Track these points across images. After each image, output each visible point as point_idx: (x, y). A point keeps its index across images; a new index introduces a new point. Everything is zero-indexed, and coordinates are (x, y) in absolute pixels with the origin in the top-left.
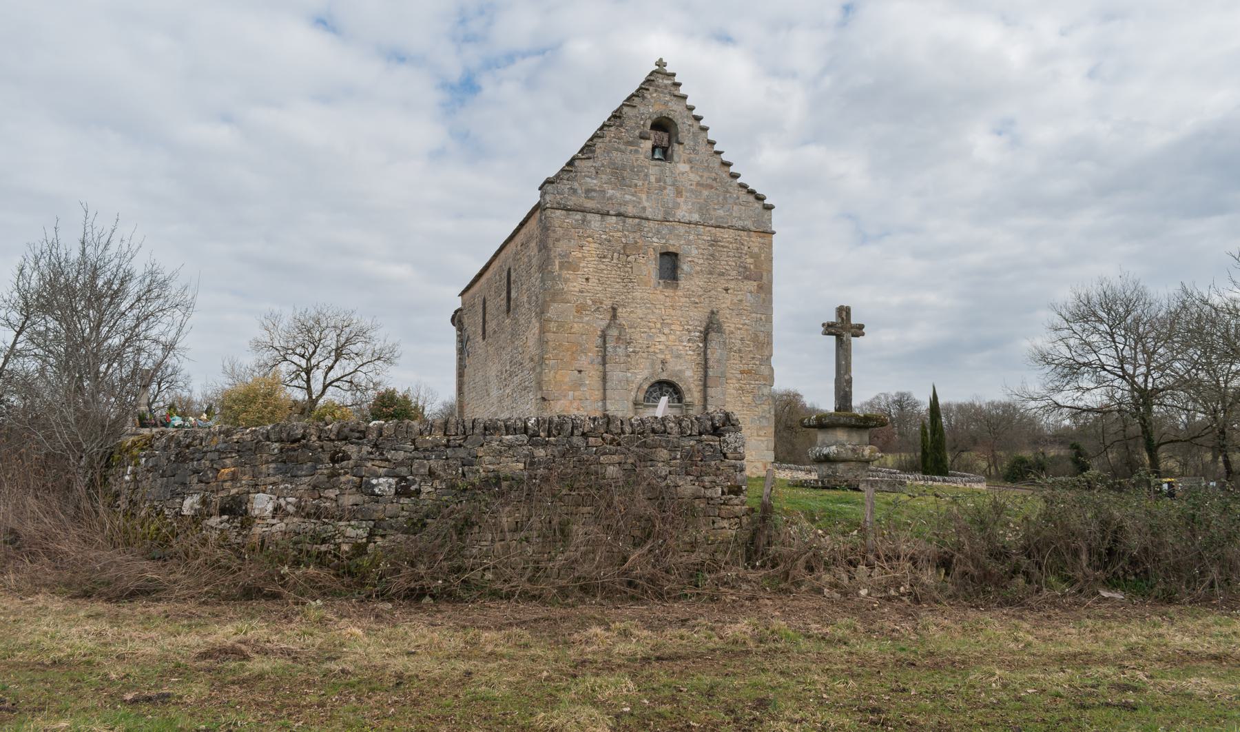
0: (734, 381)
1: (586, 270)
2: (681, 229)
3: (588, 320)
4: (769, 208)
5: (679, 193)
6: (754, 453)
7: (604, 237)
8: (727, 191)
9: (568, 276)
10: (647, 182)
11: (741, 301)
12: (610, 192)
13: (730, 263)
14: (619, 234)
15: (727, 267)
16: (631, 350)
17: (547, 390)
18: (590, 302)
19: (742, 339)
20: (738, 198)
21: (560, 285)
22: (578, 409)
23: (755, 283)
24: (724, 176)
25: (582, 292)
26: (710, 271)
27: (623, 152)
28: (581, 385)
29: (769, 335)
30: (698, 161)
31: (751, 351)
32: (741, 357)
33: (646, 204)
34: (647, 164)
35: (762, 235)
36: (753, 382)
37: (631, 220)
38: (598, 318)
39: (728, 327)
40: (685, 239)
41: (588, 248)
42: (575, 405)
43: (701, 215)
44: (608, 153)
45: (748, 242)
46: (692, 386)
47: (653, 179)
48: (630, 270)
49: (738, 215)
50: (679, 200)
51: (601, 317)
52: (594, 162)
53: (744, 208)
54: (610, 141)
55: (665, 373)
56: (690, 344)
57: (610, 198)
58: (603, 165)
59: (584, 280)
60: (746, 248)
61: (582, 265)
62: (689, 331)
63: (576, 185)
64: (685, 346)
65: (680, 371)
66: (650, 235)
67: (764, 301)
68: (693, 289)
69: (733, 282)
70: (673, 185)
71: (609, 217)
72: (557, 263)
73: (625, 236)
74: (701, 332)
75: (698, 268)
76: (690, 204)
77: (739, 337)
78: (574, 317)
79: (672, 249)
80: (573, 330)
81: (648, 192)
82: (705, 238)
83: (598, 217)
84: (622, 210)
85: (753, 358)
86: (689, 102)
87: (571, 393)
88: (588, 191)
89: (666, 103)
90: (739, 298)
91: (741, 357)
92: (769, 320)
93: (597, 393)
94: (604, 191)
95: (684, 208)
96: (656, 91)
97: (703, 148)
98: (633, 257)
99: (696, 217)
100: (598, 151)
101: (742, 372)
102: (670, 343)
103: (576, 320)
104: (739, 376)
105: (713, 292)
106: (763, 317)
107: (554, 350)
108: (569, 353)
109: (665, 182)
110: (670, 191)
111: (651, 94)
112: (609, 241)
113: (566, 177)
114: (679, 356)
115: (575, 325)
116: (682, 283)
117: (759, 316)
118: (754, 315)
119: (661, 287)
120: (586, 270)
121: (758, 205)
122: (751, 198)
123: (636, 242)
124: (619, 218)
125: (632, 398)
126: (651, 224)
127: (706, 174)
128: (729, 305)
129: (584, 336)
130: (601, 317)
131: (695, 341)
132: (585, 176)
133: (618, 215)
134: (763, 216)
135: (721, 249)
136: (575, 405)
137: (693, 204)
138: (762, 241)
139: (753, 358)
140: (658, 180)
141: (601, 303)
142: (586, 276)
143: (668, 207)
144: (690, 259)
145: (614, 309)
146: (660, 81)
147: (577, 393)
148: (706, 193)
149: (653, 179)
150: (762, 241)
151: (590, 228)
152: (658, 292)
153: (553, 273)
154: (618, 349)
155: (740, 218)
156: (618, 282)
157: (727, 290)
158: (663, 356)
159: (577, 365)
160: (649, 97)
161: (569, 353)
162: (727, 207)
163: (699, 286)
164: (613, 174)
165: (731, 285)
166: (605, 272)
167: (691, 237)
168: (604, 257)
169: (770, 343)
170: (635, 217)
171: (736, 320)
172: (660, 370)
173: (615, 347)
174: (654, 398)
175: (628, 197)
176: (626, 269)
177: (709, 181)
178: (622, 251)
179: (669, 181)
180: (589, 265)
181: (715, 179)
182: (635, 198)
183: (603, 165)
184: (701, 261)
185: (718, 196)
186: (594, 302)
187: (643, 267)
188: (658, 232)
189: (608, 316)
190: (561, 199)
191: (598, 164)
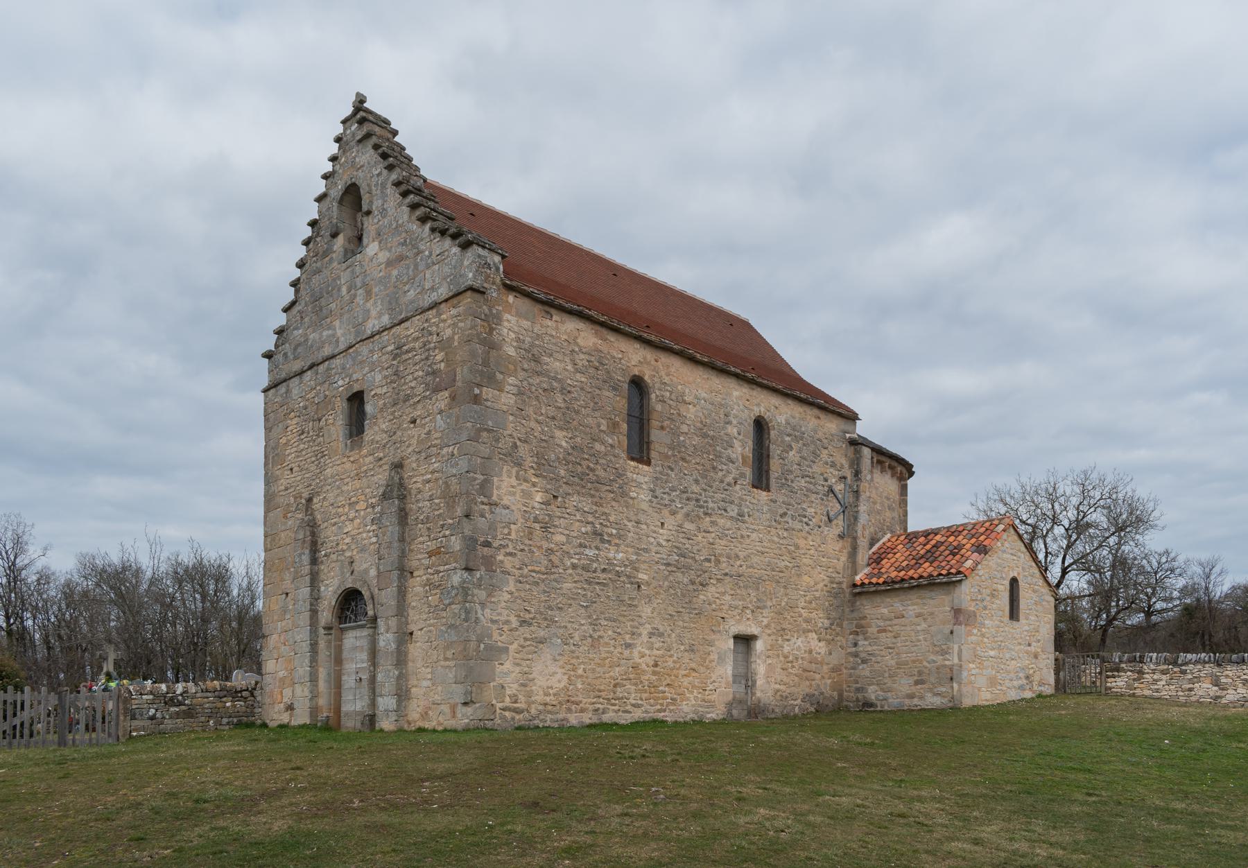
11: (429, 433)
16: (323, 553)
32: (429, 529)
35: (455, 301)
61: (287, 453)
64: (369, 531)
68: (378, 438)
69: (419, 406)
71: (305, 374)
79: (356, 388)
91: (429, 529)
101: (431, 554)
104: (426, 562)
124: (313, 370)
144: (373, 393)
157: (414, 422)
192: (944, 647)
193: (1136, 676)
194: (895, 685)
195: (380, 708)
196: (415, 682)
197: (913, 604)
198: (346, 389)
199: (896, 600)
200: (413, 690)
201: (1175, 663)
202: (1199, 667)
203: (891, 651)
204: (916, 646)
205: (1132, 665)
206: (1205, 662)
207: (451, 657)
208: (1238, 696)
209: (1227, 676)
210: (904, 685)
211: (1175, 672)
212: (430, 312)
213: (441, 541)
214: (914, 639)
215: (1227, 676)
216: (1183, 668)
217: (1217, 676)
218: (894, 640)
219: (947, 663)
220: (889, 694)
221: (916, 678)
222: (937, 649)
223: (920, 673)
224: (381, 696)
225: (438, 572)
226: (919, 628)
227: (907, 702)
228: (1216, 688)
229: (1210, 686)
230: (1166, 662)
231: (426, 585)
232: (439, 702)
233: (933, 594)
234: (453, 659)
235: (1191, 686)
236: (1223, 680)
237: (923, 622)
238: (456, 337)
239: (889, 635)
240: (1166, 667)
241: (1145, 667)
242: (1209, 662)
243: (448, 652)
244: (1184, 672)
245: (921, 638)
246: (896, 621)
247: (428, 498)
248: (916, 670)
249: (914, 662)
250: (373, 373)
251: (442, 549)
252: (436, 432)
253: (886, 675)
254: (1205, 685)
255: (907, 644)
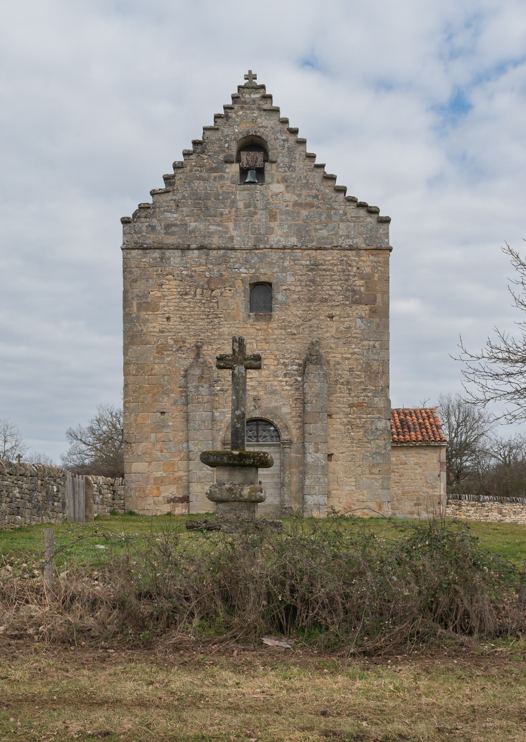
0: (342, 416)
1: (166, 309)
2: (274, 256)
3: (170, 361)
4: (386, 221)
5: (272, 217)
6: (365, 492)
7: (185, 273)
8: (332, 208)
9: (147, 316)
10: (234, 209)
11: (349, 328)
12: (193, 224)
13: (335, 287)
14: (203, 268)
15: (331, 293)
16: (219, 388)
17: (128, 433)
18: (171, 342)
19: (351, 370)
20: (345, 214)
21: (139, 327)
22: (162, 451)
23: (367, 308)
24: (327, 191)
25: (163, 332)
26: (310, 298)
27: (204, 179)
28: (163, 427)
29: (386, 363)
30: (295, 178)
31: (362, 382)
32: (350, 390)
33: (234, 233)
34: (234, 190)
35: (374, 252)
36: (365, 416)
37: (215, 252)
38: (180, 358)
39: (334, 357)
40: (279, 266)
41: (168, 286)
42: (158, 447)
43: (300, 239)
44: (189, 184)
45: (357, 263)
46: (290, 423)
47: (241, 205)
48: (215, 305)
49: (346, 233)
50: (272, 224)
51: (184, 356)
52: (174, 195)
53: (352, 224)
54: (191, 171)
55: (257, 411)
56: (287, 379)
57: (193, 231)
58: (184, 197)
59: (165, 320)
60: (355, 269)
61: (161, 304)
62: (285, 365)
63: (155, 222)
64: (281, 381)
65: (276, 408)
66: (237, 266)
67: (378, 326)
70: (266, 208)
71: (191, 252)
72: (135, 304)
73: (209, 270)
74: (299, 365)
75: (295, 297)
76: (286, 227)
77: (348, 368)
78: (155, 358)
79: (263, 279)
80: (153, 372)
81: (235, 220)
82: (303, 262)
83: (178, 253)
84: (206, 242)
85: (364, 390)
86: (282, 115)
87: (153, 435)
88: (168, 227)
89: (254, 121)
90: (346, 325)
91: (350, 390)
92: (385, 347)
93: (181, 434)
94: (186, 224)
95: (279, 232)
96: (242, 108)
97: (300, 164)
98: (218, 291)
99: (293, 240)
100: (177, 182)
101: (351, 406)
102: (262, 379)
103: (157, 361)
105: (313, 321)
106: (377, 344)
107: (134, 392)
108: (150, 395)
109: (255, 207)
110: (261, 216)
111: (236, 113)
112: (191, 277)
113: (143, 214)
114: (273, 392)
115: (156, 366)
116: (276, 314)
117: (371, 343)
118: (365, 343)
119: (251, 321)
120: (166, 309)
121: (371, 220)
122: (362, 212)
123: (221, 275)
125: (220, 438)
126: (239, 254)
127: (305, 192)
128: (333, 333)
129: (166, 377)
130: (184, 356)
131: (293, 375)
132: (164, 211)
133: (201, 248)
134: (377, 231)
135: (324, 273)
136: (158, 447)
137: (289, 227)
138: (375, 259)
139: (364, 390)
140: (248, 206)
141: (184, 342)
142: (167, 315)
143: (260, 234)
145: (198, 348)
146: (247, 96)
147: (159, 435)
148: (304, 213)
149: (241, 205)
150: (375, 259)
151: (169, 265)
152: (249, 326)
153: (131, 315)
154: (200, 388)
155: (348, 237)
156: (202, 319)
158: (255, 393)
159: (159, 407)
160: (234, 116)
161: (150, 395)
162: (331, 226)
163: (297, 316)
164: (195, 205)
165: (337, 312)
166: (188, 309)
167: (286, 264)
168: (186, 294)
169: (386, 373)
170: (219, 249)
171: (342, 349)
172: (252, 408)
173: (197, 387)
174: (250, 437)
175: (213, 228)
176: (211, 304)
177: (309, 200)
178: (206, 286)
179: (260, 204)
180: (169, 304)
181: (316, 196)
182: (220, 228)
183: (184, 197)
184: (299, 289)
185: (320, 215)
186: (176, 341)
187: (230, 301)
188: (247, 261)
189: (193, 355)
190: (139, 238)
191: (178, 197)
192: (434, 484)
193: (457, 507)
194: (401, 506)
195: (309, 503)
196: (336, 487)
197: (412, 457)
198: (251, 277)
199: (401, 453)
200: (333, 492)
201: (478, 501)
202: (492, 503)
203: (398, 484)
204: (415, 482)
205: (455, 501)
206: (494, 501)
207: (377, 472)
208: (511, 520)
209: (506, 509)
210: (408, 506)
211: (479, 506)
212: (350, 252)
213: (364, 399)
214: (413, 478)
215: (506, 509)
216: (483, 503)
217: (500, 509)
218: (400, 478)
219: (436, 493)
220: (397, 512)
221: (415, 502)
222: (429, 485)
223: (418, 499)
224: (310, 495)
225: (360, 418)
226: (416, 471)
227: (409, 516)
228: (500, 516)
229: (497, 514)
230: (473, 500)
231: (347, 425)
232: (365, 500)
233: (426, 452)
234: (379, 474)
235: (487, 514)
236: (504, 511)
237: (419, 468)
238: (376, 275)
239: (396, 474)
240: (474, 503)
241: (463, 502)
242: (496, 501)
243: (374, 469)
244: (483, 506)
245: (418, 477)
246: (401, 466)
247: (348, 370)
248: (415, 497)
249: (414, 492)
250: (284, 274)
251: (364, 404)
252: (356, 329)
253: (395, 499)
254: (494, 514)
255: (409, 481)
